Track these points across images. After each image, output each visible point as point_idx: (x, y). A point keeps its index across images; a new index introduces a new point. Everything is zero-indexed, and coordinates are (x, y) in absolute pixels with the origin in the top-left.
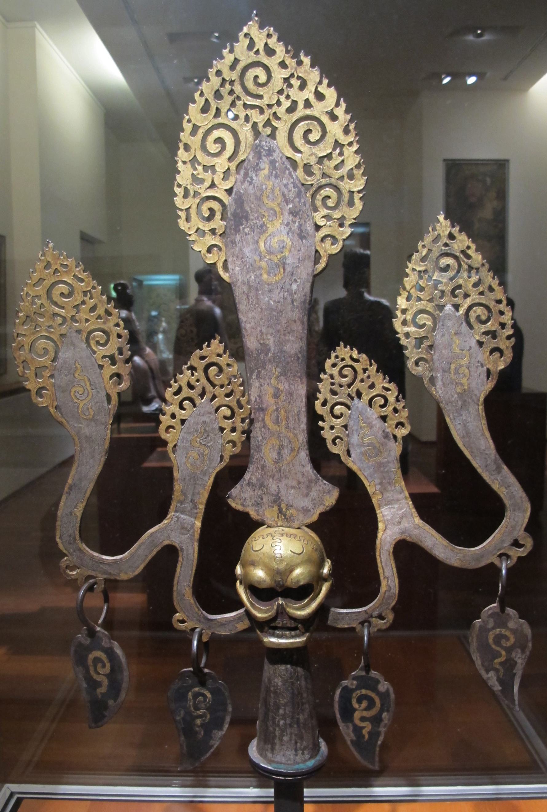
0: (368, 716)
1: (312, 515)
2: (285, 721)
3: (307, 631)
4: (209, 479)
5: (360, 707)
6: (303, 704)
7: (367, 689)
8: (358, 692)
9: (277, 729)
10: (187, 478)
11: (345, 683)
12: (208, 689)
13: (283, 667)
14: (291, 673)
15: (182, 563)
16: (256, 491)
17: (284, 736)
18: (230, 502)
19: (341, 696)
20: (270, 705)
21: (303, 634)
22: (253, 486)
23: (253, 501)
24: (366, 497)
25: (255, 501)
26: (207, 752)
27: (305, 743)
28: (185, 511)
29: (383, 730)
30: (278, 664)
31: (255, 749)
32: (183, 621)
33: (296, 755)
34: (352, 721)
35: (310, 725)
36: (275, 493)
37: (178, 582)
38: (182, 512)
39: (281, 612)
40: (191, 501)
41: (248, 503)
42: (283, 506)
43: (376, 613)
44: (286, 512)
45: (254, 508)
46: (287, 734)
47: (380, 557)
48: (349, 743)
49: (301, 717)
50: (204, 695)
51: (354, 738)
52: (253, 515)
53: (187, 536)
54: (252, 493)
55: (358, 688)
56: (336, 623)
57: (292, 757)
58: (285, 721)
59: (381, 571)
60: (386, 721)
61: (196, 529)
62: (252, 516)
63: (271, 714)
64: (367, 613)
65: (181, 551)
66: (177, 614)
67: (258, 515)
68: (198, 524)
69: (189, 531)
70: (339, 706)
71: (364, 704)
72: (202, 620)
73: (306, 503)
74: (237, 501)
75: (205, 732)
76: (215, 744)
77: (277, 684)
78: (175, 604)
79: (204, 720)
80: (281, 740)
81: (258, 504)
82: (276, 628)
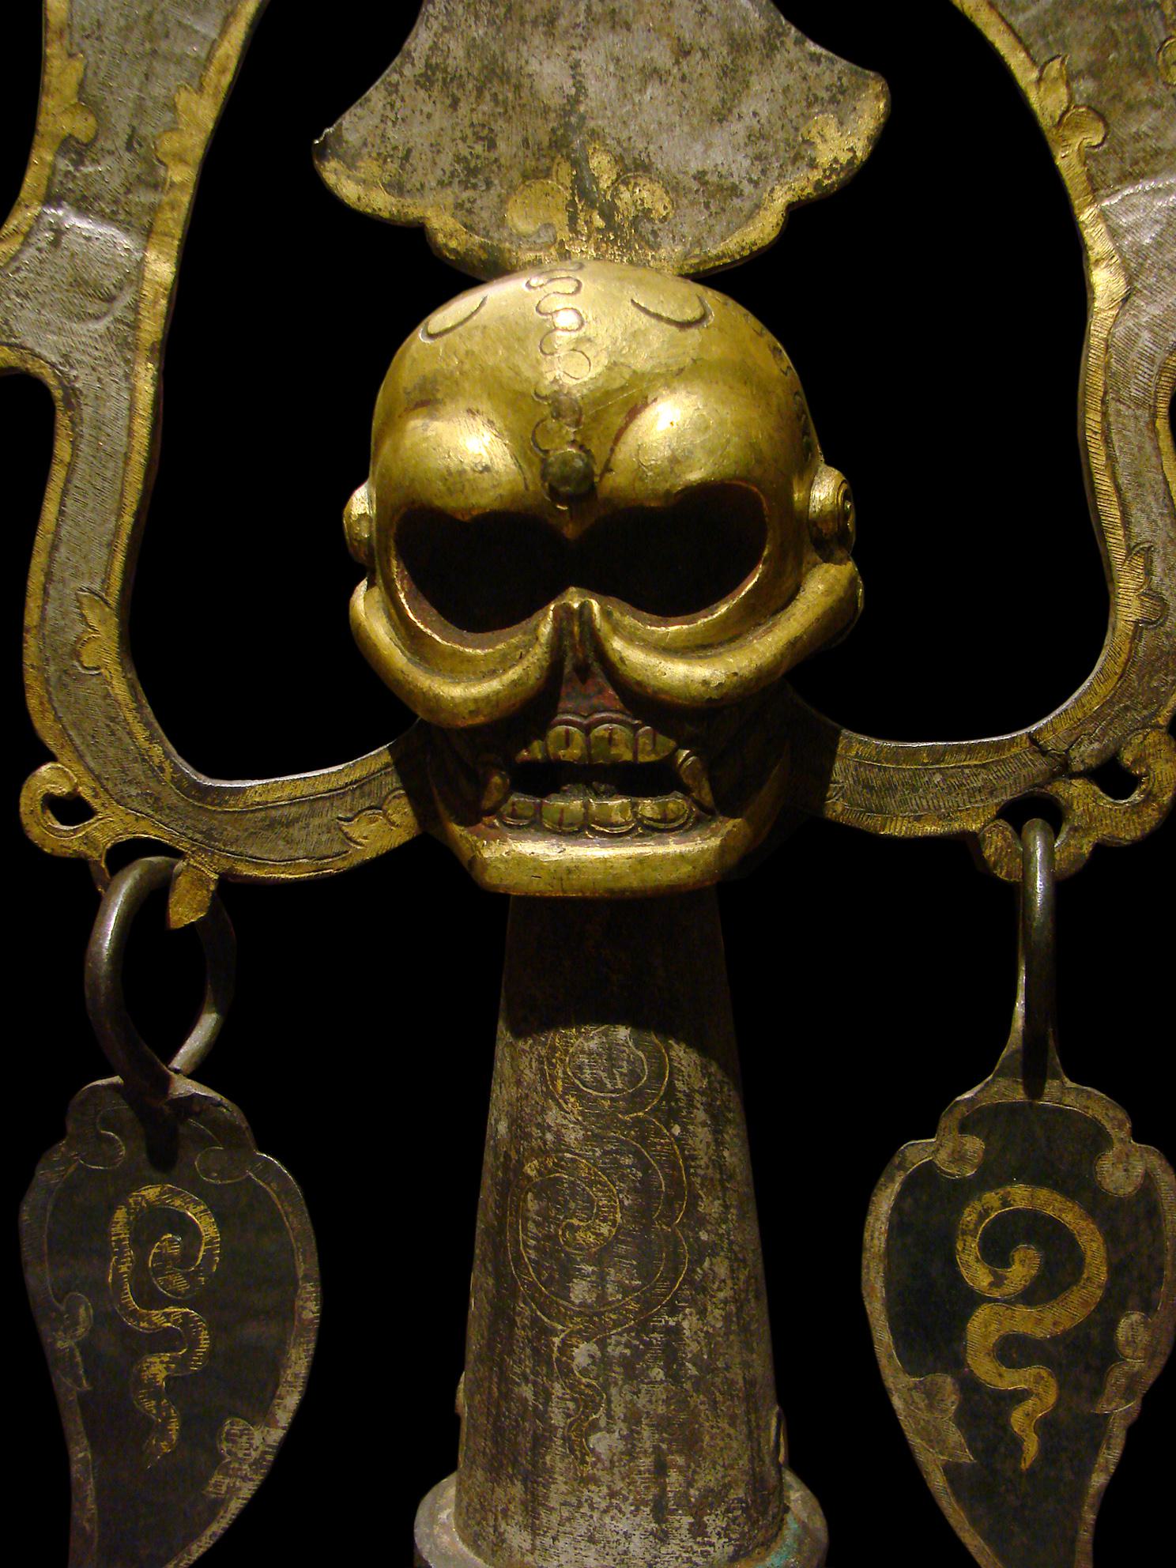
0: (1040, 1333)
1: (750, 217)
2: (602, 1344)
3: (724, 805)
4: (223, 32)
5: (998, 1281)
6: (701, 1252)
7: (1036, 1180)
8: (991, 1198)
9: (558, 1389)
10: (115, 21)
11: (917, 1152)
12: (203, 1193)
13: (588, 1040)
14: (634, 1076)
15: (71, 468)
16: (464, 109)
17: (594, 1427)
18: (330, 178)
19: (899, 1224)
20: (518, 1258)
21: (702, 818)
22: (452, 80)
23: (446, 160)
24: (1029, 143)
25: (459, 159)
26: (194, 1536)
27: (708, 1479)
28: (97, 198)
29: (1119, 1410)
30: (567, 1025)
31: (446, 1515)
32: (71, 809)
33: (663, 1537)
34: (955, 1363)
35: (737, 1375)
36: (556, 101)
37: (49, 575)
38: (83, 206)
39: (580, 662)
40: (129, 147)
41: (423, 172)
42: (601, 165)
43: (1086, 753)
44: (616, 194)
45: (449, 196)
46: (609, 1415)
47: (1107, 440)
48: (937, 1481)
49: (689, 1323)
50: (187, 1229)
51: (967, 1457)
52: (448, 231)
53: (100, 326)
54: (441, 120)
55: (990, 1176)
56: (880, 810)
57: (637, 1546)
58: (602, 1344)
59: (1110, 511)
60: (1135, 1362)
61: (148, 291)
62: (441, 239)
63: (524, 1310)
64: (1044, 752)
65: (69, 406)
66: (45, 770)
67: (470, 228)
68: (162, 268)
69: (110, 299)
70: (888, 1283)
71: (1022, 1268)
72: (172, 796)
73: (722, 154)
74: (368, 167)
75: (185, 1424)
76: (232, 1491)
77: (559, 1137)
78: (32, 702)
79: (183, 1363)
80: (578, 1450)
81: (473, 172)
82: (547, 779)
